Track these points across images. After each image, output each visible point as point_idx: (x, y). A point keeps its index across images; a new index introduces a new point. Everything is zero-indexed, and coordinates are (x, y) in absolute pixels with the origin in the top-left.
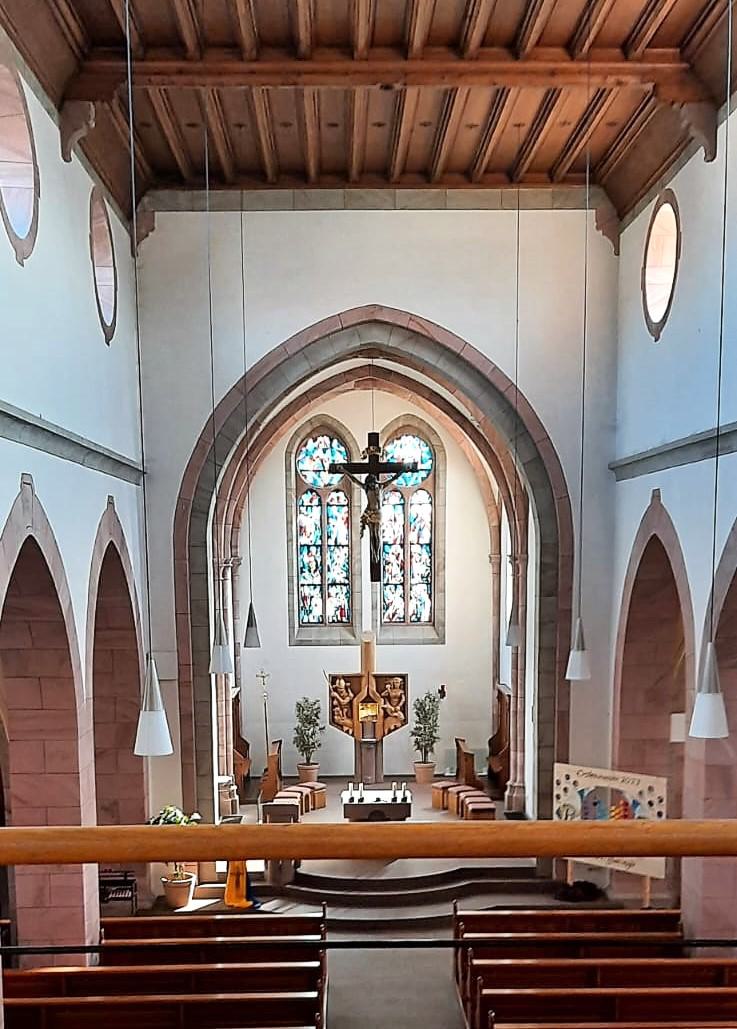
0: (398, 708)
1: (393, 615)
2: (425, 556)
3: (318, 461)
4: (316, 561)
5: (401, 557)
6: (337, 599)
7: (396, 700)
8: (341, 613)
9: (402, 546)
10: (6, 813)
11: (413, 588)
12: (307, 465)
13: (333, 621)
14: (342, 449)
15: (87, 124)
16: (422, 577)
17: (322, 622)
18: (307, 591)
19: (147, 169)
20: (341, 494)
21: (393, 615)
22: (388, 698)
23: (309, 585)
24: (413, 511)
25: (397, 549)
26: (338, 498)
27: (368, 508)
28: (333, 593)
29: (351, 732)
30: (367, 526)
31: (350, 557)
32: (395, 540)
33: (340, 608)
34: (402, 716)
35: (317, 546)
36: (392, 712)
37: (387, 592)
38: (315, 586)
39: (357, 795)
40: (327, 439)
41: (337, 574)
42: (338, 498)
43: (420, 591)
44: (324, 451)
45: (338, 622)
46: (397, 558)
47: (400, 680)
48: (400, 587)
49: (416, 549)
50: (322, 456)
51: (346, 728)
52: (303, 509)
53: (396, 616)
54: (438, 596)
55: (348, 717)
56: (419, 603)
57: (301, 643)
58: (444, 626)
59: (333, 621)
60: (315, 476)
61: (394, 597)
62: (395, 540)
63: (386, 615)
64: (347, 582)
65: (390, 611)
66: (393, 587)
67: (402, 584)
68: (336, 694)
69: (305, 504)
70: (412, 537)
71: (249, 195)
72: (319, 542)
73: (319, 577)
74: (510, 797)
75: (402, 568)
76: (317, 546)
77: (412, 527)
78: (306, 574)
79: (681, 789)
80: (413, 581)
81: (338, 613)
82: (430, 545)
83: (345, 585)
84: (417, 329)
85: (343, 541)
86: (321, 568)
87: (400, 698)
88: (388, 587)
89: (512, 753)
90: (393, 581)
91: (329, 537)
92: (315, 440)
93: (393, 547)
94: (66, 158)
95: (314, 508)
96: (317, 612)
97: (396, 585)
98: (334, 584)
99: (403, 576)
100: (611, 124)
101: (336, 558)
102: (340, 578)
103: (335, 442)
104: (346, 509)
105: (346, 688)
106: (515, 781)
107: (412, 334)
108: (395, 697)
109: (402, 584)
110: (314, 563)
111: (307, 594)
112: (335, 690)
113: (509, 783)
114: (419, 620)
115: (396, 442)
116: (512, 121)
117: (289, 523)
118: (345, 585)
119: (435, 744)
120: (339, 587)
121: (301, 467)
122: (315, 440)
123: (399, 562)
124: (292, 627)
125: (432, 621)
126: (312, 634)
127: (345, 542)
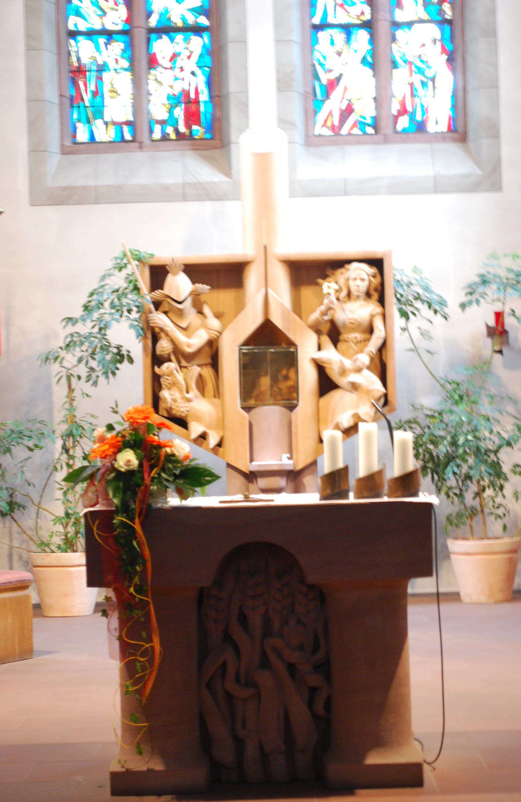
10: (114, 599)
11: (399, 34)
13: (165, 138)
28: (163, 57)
38: (109, 34)
45: (180, 136)
47: (366, 270)
56: (417, 79)
64: (203, 21)
67: (368, 25)
79: (227, 200)
81: (179, 113)
83: (197, 30)
87: (370, 330)
88: (323, 35)
109: (368, 25)
111: (85, 60)
118: (197, 30)
119: (82, 333)
120: (179, 37)
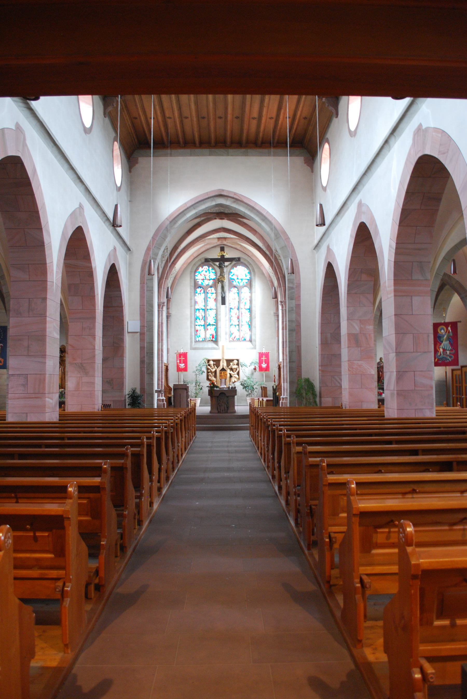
1: (234, 338)
3: (203, 276)
4: (202, 316)
6: (211, 330)
7: (235, 370)
9: (238, 309)
13: (209, 340)
14: (213, 271)
15: (113, 105)
16: (246, 322)
17: (205, 340)
18: (197, 328)
19: (136, 140)
21: (234, 338)
22: (232, 369)
23: (199, 325)
24: (242, 296)
25: (236, 311)
26: (211, 290)
27: (221, 275)
30: (219, 283)
32: (235, 307)
41: (211, 320)
42: (211, 290)
43: (245, 328)
44: (206, 272)
45: (211, 340)
46: (236, 314)
50: (205, 274)
53: (235, 338)
54: (253, 329)
55: (214, 377)
57: (195, 349)
59: (209, 340)
60: (202, 281)
61: (234, 330)
62: (235, 307)
63: (231, 338)
64: (215, 324)
65: (233, 336)
68: (209, 367)
69: (198, 293)
70: (242, 306)
71: (174, 151)
72: (204, 308)
74: (282, 403)
78: (198, 321)
82: (249, 309)
84: (237, 198)
86: (205, 318)
87: (237, 369)
92: (202, 267)
94: (105, 117)
95: (202, 294)
98: (209, 325)
99: (239, 322)
100: (305, 118)
103: (210, 268)
105: (214, 365)
106: (284, 395)
107: (235, 200)
108: (234, 369)
112: (209, 365)
113: (281, 397)
114: (245, 340)
116: (269, 116)
117: (191, 299)
118: (214, 325)
122: (202, 267)
124: (191, 342)
126: (199, 345)
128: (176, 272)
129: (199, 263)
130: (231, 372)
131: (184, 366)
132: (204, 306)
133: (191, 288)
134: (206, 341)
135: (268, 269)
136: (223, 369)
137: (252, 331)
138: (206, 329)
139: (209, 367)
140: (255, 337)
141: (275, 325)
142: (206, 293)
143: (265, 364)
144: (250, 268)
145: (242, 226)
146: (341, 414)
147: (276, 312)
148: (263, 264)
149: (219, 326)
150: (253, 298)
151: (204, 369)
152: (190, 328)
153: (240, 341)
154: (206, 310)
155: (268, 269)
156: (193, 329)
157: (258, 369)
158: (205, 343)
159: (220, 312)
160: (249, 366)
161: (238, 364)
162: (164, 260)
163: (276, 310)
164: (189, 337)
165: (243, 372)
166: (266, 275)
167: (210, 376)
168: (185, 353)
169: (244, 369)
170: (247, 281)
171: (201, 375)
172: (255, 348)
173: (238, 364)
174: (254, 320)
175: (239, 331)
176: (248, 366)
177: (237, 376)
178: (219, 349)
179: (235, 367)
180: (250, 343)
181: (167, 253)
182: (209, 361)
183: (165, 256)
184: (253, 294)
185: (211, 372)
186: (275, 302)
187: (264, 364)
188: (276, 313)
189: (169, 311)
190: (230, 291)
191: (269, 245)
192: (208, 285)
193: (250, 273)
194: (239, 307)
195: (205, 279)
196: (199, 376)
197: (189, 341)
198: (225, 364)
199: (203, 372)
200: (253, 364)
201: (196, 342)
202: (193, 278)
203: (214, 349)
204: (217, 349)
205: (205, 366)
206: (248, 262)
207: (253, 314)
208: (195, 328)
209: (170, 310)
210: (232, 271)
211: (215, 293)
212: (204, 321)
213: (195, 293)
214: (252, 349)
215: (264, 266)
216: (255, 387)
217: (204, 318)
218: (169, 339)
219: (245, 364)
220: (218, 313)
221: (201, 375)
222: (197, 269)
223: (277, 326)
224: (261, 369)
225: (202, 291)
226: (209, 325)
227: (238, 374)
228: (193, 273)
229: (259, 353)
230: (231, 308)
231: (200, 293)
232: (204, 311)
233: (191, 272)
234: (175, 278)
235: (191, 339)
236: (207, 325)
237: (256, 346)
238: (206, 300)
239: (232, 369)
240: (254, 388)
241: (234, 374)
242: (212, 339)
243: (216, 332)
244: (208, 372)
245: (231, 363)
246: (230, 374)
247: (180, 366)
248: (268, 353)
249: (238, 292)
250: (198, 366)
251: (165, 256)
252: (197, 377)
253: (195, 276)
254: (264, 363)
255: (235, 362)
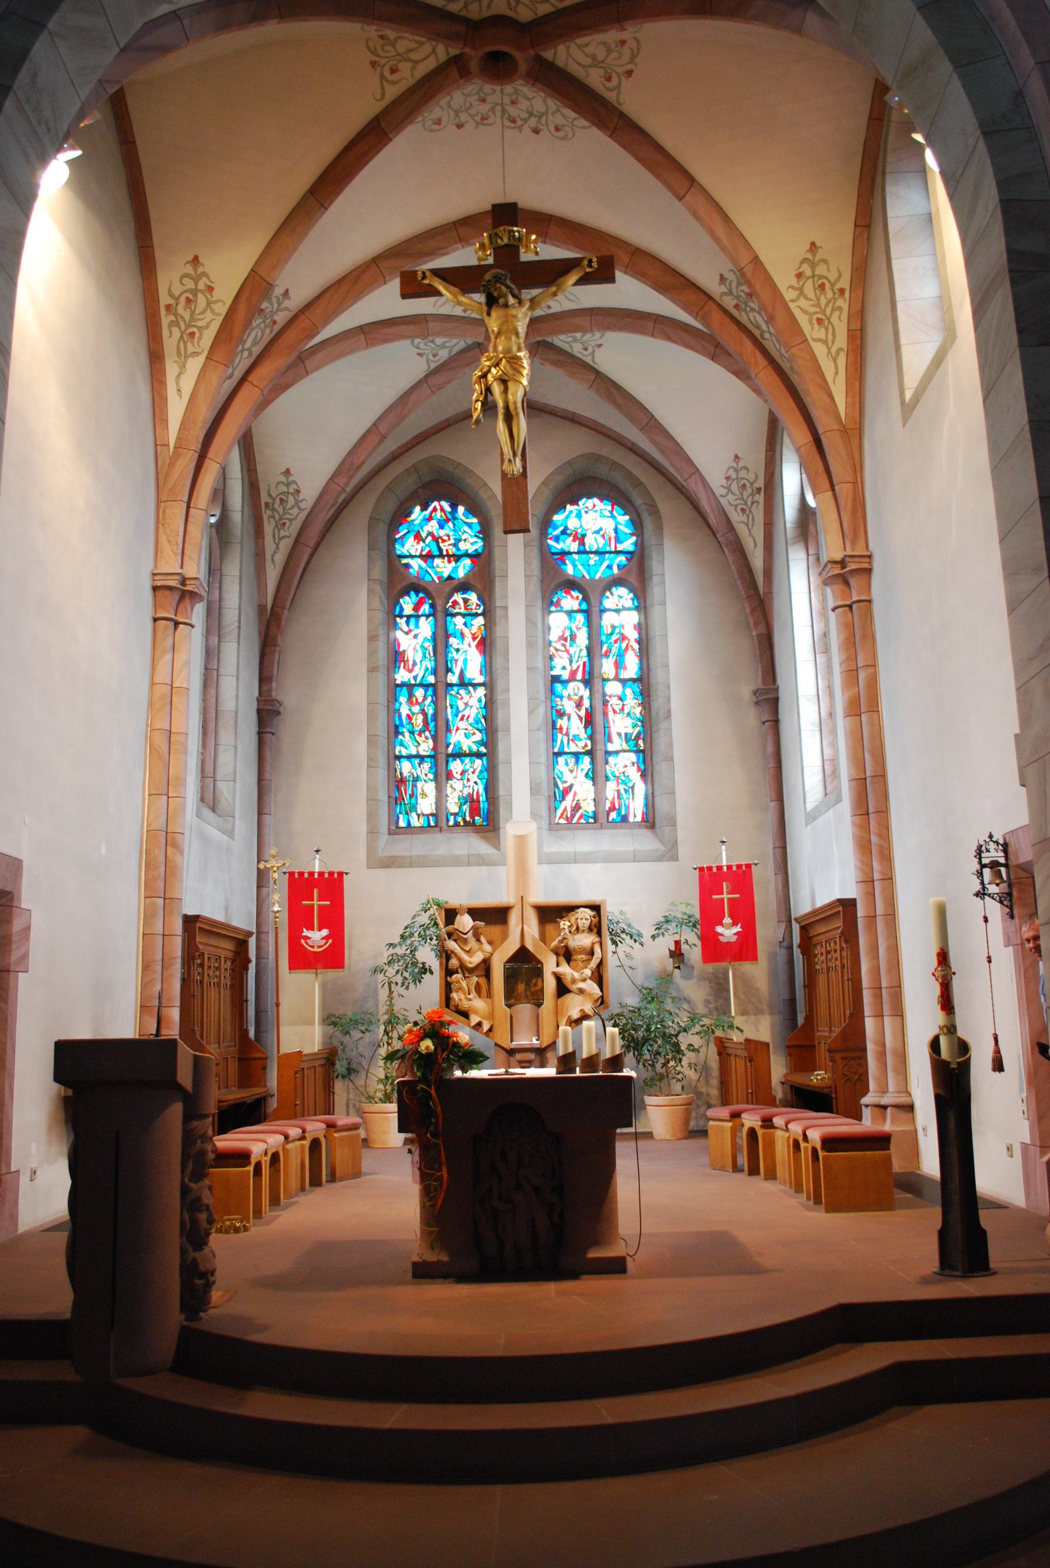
0: (588, 972)
2: (632, 703)
4: (423, 713)
5: (586, 703)
8: (471, 810)
9: (587, 682)
11: (611, 759)
12: (409, 546)
16: (627, 741)
17: (438, 822)
18: (406, 768)
20: (473, 597)
22: (567, 954)
25: (578, 689)
29: (486, 1027)
31: (490, 705)
33: (472, 801)
34: (596, 990)
35: (426, 686)
36: (574, 981)
37: (562, 765)
38: (422, 758)
39: (453, 801)
40: (446, 505)
42: (466, 601)
48: (587, 759)
49: (613, 688)
51: (474, 1019)
52: (401, 622)
54: (661, 768)
57: (390, 863)
58: (674, 825)
59: (457, 824)
64: (483, 749)
65: (568, 803)
66: (572, 761)
68: (452, 945)
69: (406, 612)
72: (431, 679)
73: (431, 743)
75: (589, 720)
76: (426, 686)
77: (605, 648)
80: (611, 747)
85: (474, 674)
87: (592, 953)
88: (561, 760)
89: (870, 1024)
90: (573, 748)
91: (448, 670)
92: (424, 508)
93: (571, 685)
96: (427, 805)
97: (576, 755)
98: (459, 755)
99: (591, 738)
101: (461, 706)
102: (468, 744)
104: (481, 620)
106: (884, 1090)
108: (582, 950)
110: (421, 717)
111: (406, 774)
114: (625, 819)
115: (569, 507)
120: (467, 760)
121: (400, 550)
123: (583, 713)
124: (372, 832)
125: (649, 821)
126: (404, 846)
127: (481, 679)
128: (303, 516)
129: (411, 483)
130: (565, 969)
131: (326, 938)
132: (435, 672)
133: (370, 591)
134: (444, 825)
135: (724, 491)
136: (523, 955)
137: (656, 777)
138: (442, 777)
139: (452, 945)
140: (673, 803)
141: (764, 747)
142: (441, 614)
143: (734, 924)
144: (638, 501)
145: (613, 133)
146: (219, 1017)
147: (764, 683)
148: (698, 470)
149: (501, 756)
150: (656, 630)
151: (427, 955)
152: (369, 766)
153: (602, 827)
154: (441, 688)
155: (724, 491)
156: (382, 774)
157: (694, 953)
158: (439, 837)
159: (507, 690)
160: (653, 937)
161: (596, 928)
162: (196, 354)
163: (764, 679)
164: (362, 808)
165: (622, 966)
166: (712, 519)
167: (460, 989)
168: (331, 874)
169: (628, 950)
170: (622, 559)
171: (412, 985)
172: (671, 853)
173: (596, 928)
174: (663, 726)
175: (593, 779)
176: (646, 939)
177: (592, 987)
178: (503, 863)
179: (585, 940)
180: (646, 833)
181: (209, 316)
182: (451, 915)
183: (291, 520)
184: (655, 612)
185: (463, 968)
186: (760, 642)
187: (728, 927)
188: (767, 691)
189: (270, 691)
190: (552, 603)
191: (757, 256)
192: (450, 578)
193: (637, 525)
194: (591, 673)
195: (436, 552)
196: (402, 990)
197: (363, 829)
198: (532, 928)
199: (425, 970)
200: (672, 927)
201: (395, 830)
202: (384, 547)
203: (482, 861)
204: (492, 863)
205: (434, 942)
206: (629, 475)
207: (657, 703)
208: (391, 770)
209: (274, 685)
210: (557, 518)
211: (483, 614)
212: (435, 738)
213: (393, 615)
214: (660, 859)
215: (700, 473)
216: (684, 1040)
217: (432, 725)
218: (267, 819)
219: (629, 926)
220: (499, 697)
221: (412, 985)
222: (401, 515)
223: (770, 749)
224: (713, 949)
225: (426, 608)
226: (459, 755)
227: (599, 977)
228: (382, 529)
229: (701, 869)
230: (556, 679)
231: (418, 617)
232: (435, 694)
233: (373, 521)
234: (297, 541)
235: (371, 816)
236: (449, 756)
237: (675, 844)
238: (441, 641)
239: (567, 954)
240: (683, 1047)
241: (576, 975)
242: (472, 816)
243: (491, 787)
244: (449, 972)
245: (564, 924)
246: (558, 978)
247: (306, 938)
248: (748, 866)
249: (584, 606)
250: (397, 940)
251: (291, 520)
252: (395, 994)
253: (391, 542)
254: (727, 920)
255: (585, 916)
